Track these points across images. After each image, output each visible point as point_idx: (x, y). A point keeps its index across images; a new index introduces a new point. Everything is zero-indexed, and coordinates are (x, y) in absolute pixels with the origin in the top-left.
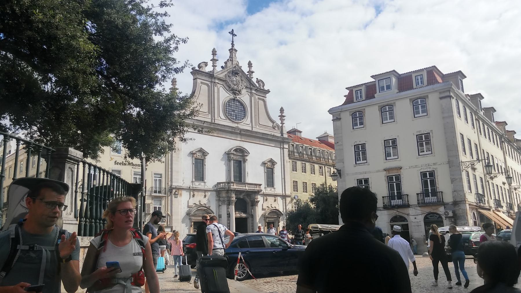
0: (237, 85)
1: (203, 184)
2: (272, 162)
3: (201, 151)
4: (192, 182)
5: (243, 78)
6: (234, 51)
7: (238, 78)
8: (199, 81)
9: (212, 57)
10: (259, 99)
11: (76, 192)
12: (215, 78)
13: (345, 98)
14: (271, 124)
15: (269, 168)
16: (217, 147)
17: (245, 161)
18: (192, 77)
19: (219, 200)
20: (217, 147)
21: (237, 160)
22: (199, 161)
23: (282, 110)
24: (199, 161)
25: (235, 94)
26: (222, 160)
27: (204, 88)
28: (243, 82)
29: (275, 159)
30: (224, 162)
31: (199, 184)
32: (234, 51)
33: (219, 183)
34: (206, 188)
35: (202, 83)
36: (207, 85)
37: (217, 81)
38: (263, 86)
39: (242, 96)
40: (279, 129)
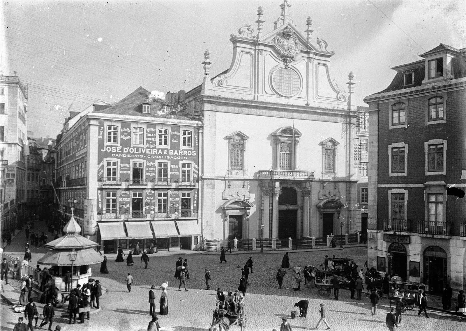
0: (289, 50)
1: (241, 172)
2: (334, 143)
3: (243, 137)
4: (228, 171)
5: (297, 41)
6: (286, 7)
7: (291, 41)
8: (239, 50)
9: (257, 27)
10: (319, 64)
11: (436, 52)
12: (259, 44)
13: (395, 73)
14: (334, 95)
15: (330, 149)
16: (258, 129)
17: (296, 143)
18: (231, 45)
19: (261, 190)
20: (258, 129)
21: (286, 141)
22: (238, 143)
23: (351, 76)
24: (238, 143)
25: (285, 61)
26: (268, 139)
27: (247, 58)
28: (298, 45)
29: (337, 139)
30: (270, 141)
31: (237, 173)
32: (286, 7)
33: (260, 172)
34: (246, 177)
35: (243, 52)
36: (250, 53)
37: (262, 47)
38: (326, 48)
39: (295, 63)
40: (345, 100)
